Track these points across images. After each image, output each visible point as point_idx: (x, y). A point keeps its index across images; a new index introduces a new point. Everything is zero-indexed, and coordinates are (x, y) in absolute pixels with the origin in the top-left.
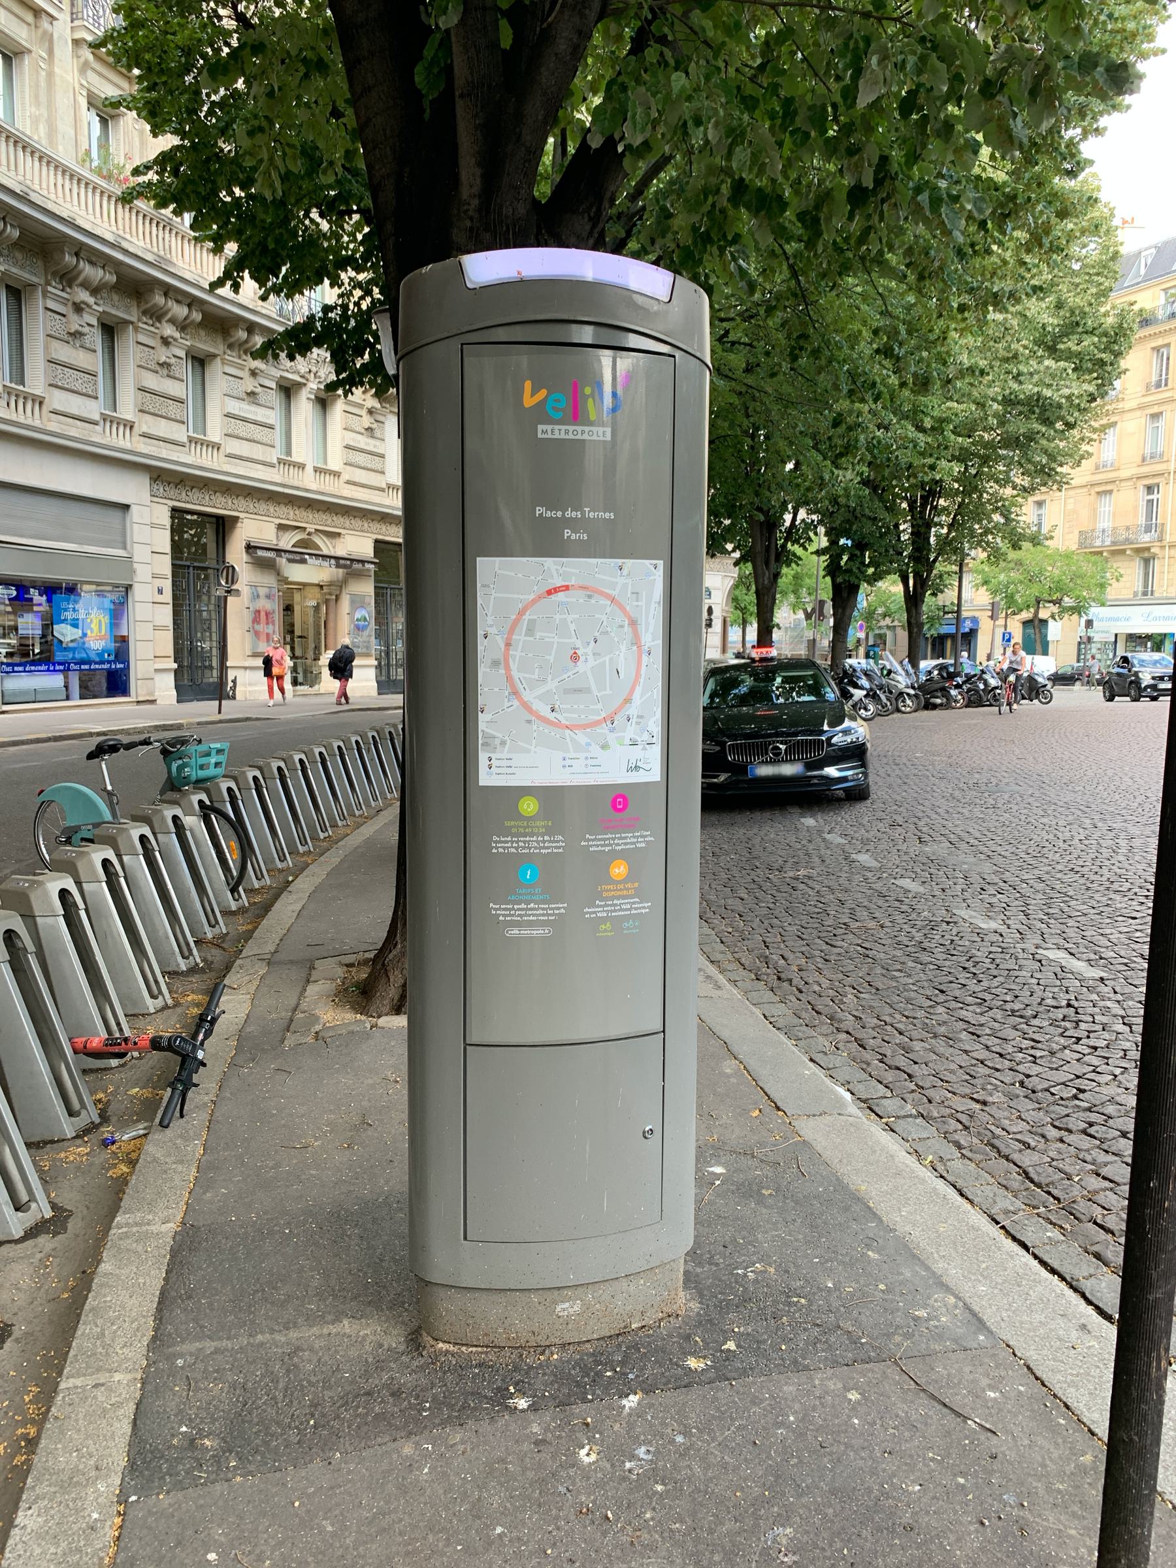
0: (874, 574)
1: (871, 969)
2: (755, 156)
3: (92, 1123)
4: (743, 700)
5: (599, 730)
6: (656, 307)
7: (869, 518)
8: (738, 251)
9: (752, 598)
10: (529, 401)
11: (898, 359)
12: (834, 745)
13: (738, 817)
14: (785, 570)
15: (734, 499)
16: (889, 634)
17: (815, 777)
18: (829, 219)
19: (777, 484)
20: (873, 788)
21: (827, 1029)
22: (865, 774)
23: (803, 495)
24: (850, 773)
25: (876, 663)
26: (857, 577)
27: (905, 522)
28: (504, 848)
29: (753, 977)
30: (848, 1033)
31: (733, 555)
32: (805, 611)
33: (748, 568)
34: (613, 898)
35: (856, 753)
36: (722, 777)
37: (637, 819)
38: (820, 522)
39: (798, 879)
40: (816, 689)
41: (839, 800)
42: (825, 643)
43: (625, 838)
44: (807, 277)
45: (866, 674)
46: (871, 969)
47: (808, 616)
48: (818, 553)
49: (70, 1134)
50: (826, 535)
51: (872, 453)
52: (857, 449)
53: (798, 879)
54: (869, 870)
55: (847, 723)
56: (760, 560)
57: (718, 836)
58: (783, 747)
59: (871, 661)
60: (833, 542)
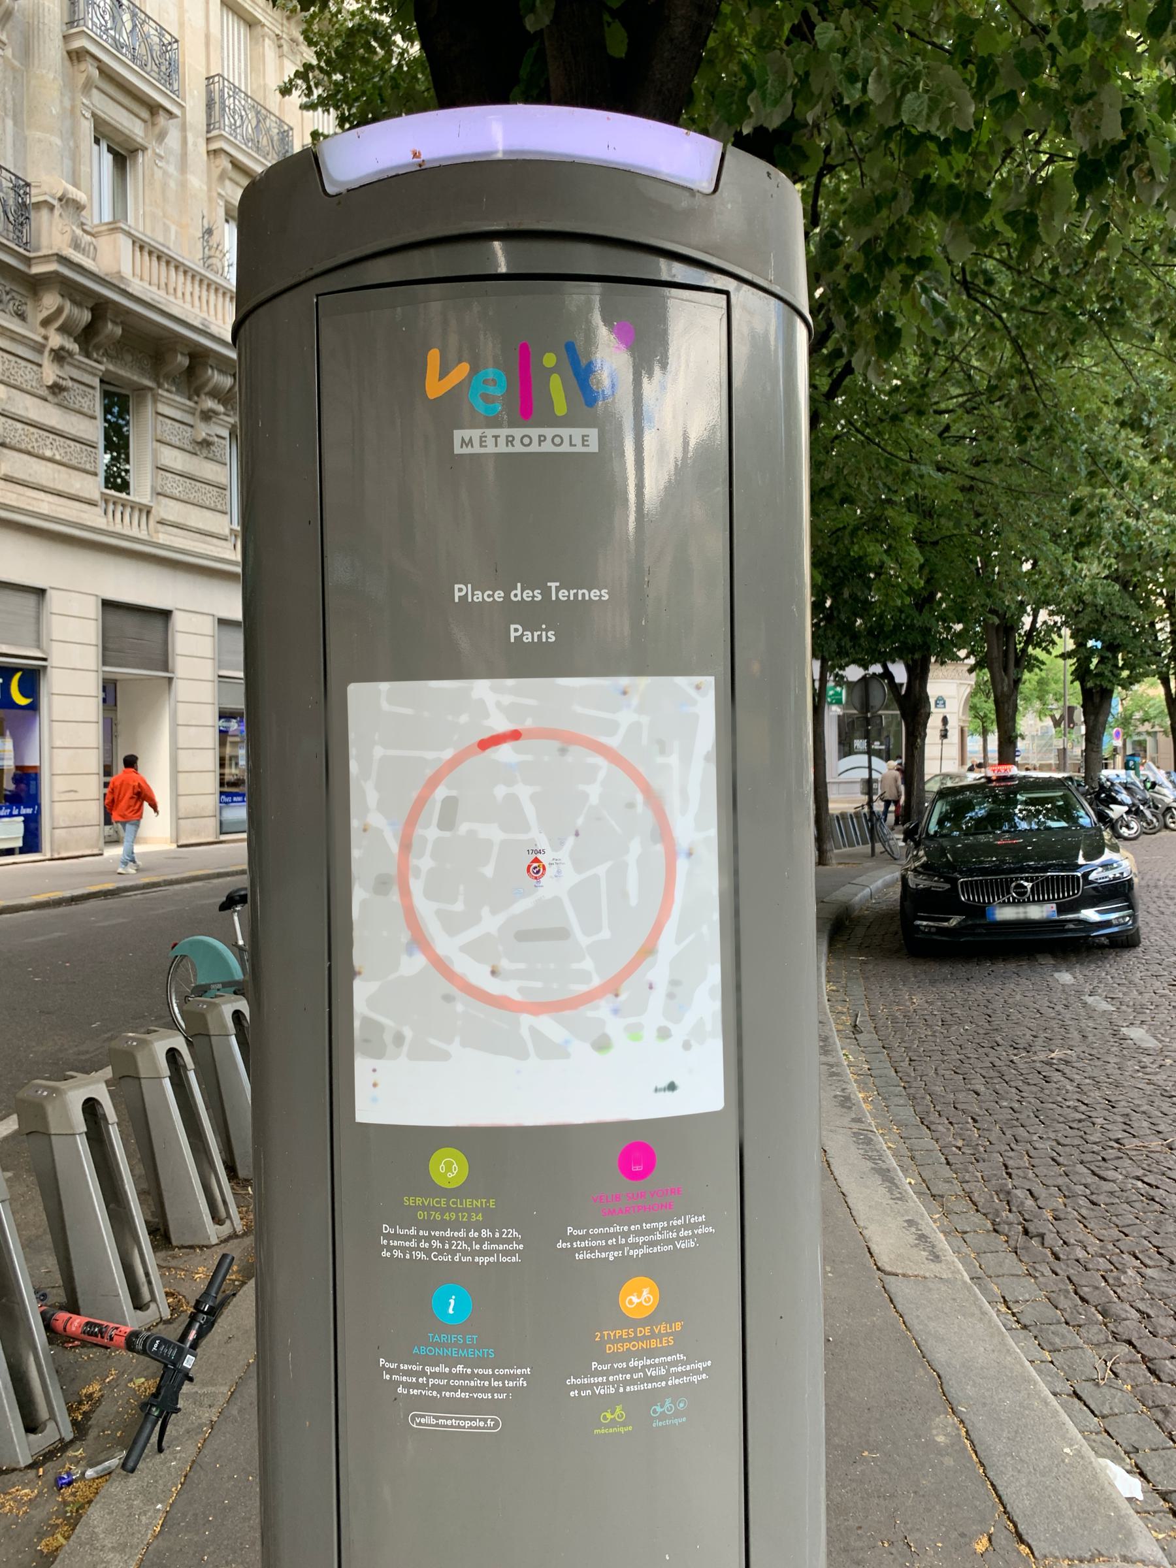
0: (1129, 677)
1: (1159, 1223)
2: (934, 104)
3: (61, 1440)
4: (981, 825)
5: (589, 1012)
6: (685, 203)
7: (1121, 617)
8: (927, 279)
9: (991, 705)
10: (435, 387)
11: (1148, 430)
12: (1092, 882)
13: (975, 970)
14: (1026, 675)
15: (964, 602)
16: (1150, 742)
17: (1070, 921)
18: (1049, 217)
19: (1011, 583)
20: (1144, 931)
21: (1097, 1333)
22: (1134, 917)
23: (1043, 594)
24: (1112, 916)
25: (1137, 774)
26: (1110, 681)
27: (1162, 620)
28: (403, 1249)
29: (989, 1226)
30: (1130, 1343)
31: (966, 661)
32: (1053, 717)
33: (986, 675)
34: (627, 1356)
35: (1119, 892)
36: (954, 921)
37: (676, 1191)
38: (1064, 623)
39: (1051, 1064)
40: (1066, 812)
41: (1102, 947)
42: (1077, 750)
43: (652, 1232)
44: (1034, 351)
45: (1126, 788)
46: (1159, 1223)
47: (1057, 724)
48: (1064, 656)
49: (24, 1460)
50: (1072, 637)
51: (1120, 542)
52: (1101, 537)
53: (1051, 1064)
54: (1146, 1052)
55: (1108, 855)
56: (997, 666)
57: (950, 996)
58: (1028, 885)
59: (1132, 772)
60: (1081, 645)
